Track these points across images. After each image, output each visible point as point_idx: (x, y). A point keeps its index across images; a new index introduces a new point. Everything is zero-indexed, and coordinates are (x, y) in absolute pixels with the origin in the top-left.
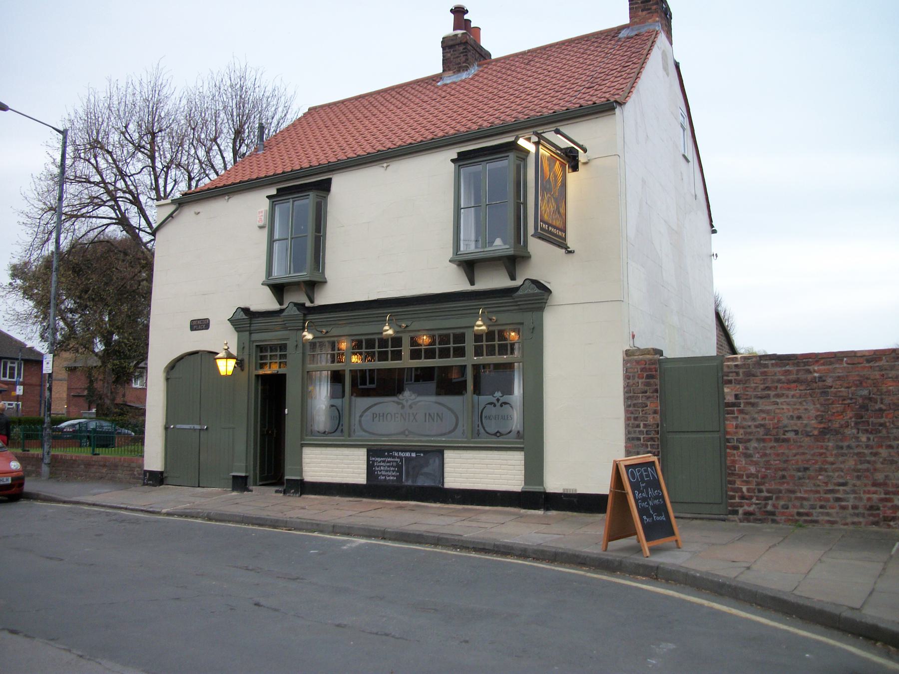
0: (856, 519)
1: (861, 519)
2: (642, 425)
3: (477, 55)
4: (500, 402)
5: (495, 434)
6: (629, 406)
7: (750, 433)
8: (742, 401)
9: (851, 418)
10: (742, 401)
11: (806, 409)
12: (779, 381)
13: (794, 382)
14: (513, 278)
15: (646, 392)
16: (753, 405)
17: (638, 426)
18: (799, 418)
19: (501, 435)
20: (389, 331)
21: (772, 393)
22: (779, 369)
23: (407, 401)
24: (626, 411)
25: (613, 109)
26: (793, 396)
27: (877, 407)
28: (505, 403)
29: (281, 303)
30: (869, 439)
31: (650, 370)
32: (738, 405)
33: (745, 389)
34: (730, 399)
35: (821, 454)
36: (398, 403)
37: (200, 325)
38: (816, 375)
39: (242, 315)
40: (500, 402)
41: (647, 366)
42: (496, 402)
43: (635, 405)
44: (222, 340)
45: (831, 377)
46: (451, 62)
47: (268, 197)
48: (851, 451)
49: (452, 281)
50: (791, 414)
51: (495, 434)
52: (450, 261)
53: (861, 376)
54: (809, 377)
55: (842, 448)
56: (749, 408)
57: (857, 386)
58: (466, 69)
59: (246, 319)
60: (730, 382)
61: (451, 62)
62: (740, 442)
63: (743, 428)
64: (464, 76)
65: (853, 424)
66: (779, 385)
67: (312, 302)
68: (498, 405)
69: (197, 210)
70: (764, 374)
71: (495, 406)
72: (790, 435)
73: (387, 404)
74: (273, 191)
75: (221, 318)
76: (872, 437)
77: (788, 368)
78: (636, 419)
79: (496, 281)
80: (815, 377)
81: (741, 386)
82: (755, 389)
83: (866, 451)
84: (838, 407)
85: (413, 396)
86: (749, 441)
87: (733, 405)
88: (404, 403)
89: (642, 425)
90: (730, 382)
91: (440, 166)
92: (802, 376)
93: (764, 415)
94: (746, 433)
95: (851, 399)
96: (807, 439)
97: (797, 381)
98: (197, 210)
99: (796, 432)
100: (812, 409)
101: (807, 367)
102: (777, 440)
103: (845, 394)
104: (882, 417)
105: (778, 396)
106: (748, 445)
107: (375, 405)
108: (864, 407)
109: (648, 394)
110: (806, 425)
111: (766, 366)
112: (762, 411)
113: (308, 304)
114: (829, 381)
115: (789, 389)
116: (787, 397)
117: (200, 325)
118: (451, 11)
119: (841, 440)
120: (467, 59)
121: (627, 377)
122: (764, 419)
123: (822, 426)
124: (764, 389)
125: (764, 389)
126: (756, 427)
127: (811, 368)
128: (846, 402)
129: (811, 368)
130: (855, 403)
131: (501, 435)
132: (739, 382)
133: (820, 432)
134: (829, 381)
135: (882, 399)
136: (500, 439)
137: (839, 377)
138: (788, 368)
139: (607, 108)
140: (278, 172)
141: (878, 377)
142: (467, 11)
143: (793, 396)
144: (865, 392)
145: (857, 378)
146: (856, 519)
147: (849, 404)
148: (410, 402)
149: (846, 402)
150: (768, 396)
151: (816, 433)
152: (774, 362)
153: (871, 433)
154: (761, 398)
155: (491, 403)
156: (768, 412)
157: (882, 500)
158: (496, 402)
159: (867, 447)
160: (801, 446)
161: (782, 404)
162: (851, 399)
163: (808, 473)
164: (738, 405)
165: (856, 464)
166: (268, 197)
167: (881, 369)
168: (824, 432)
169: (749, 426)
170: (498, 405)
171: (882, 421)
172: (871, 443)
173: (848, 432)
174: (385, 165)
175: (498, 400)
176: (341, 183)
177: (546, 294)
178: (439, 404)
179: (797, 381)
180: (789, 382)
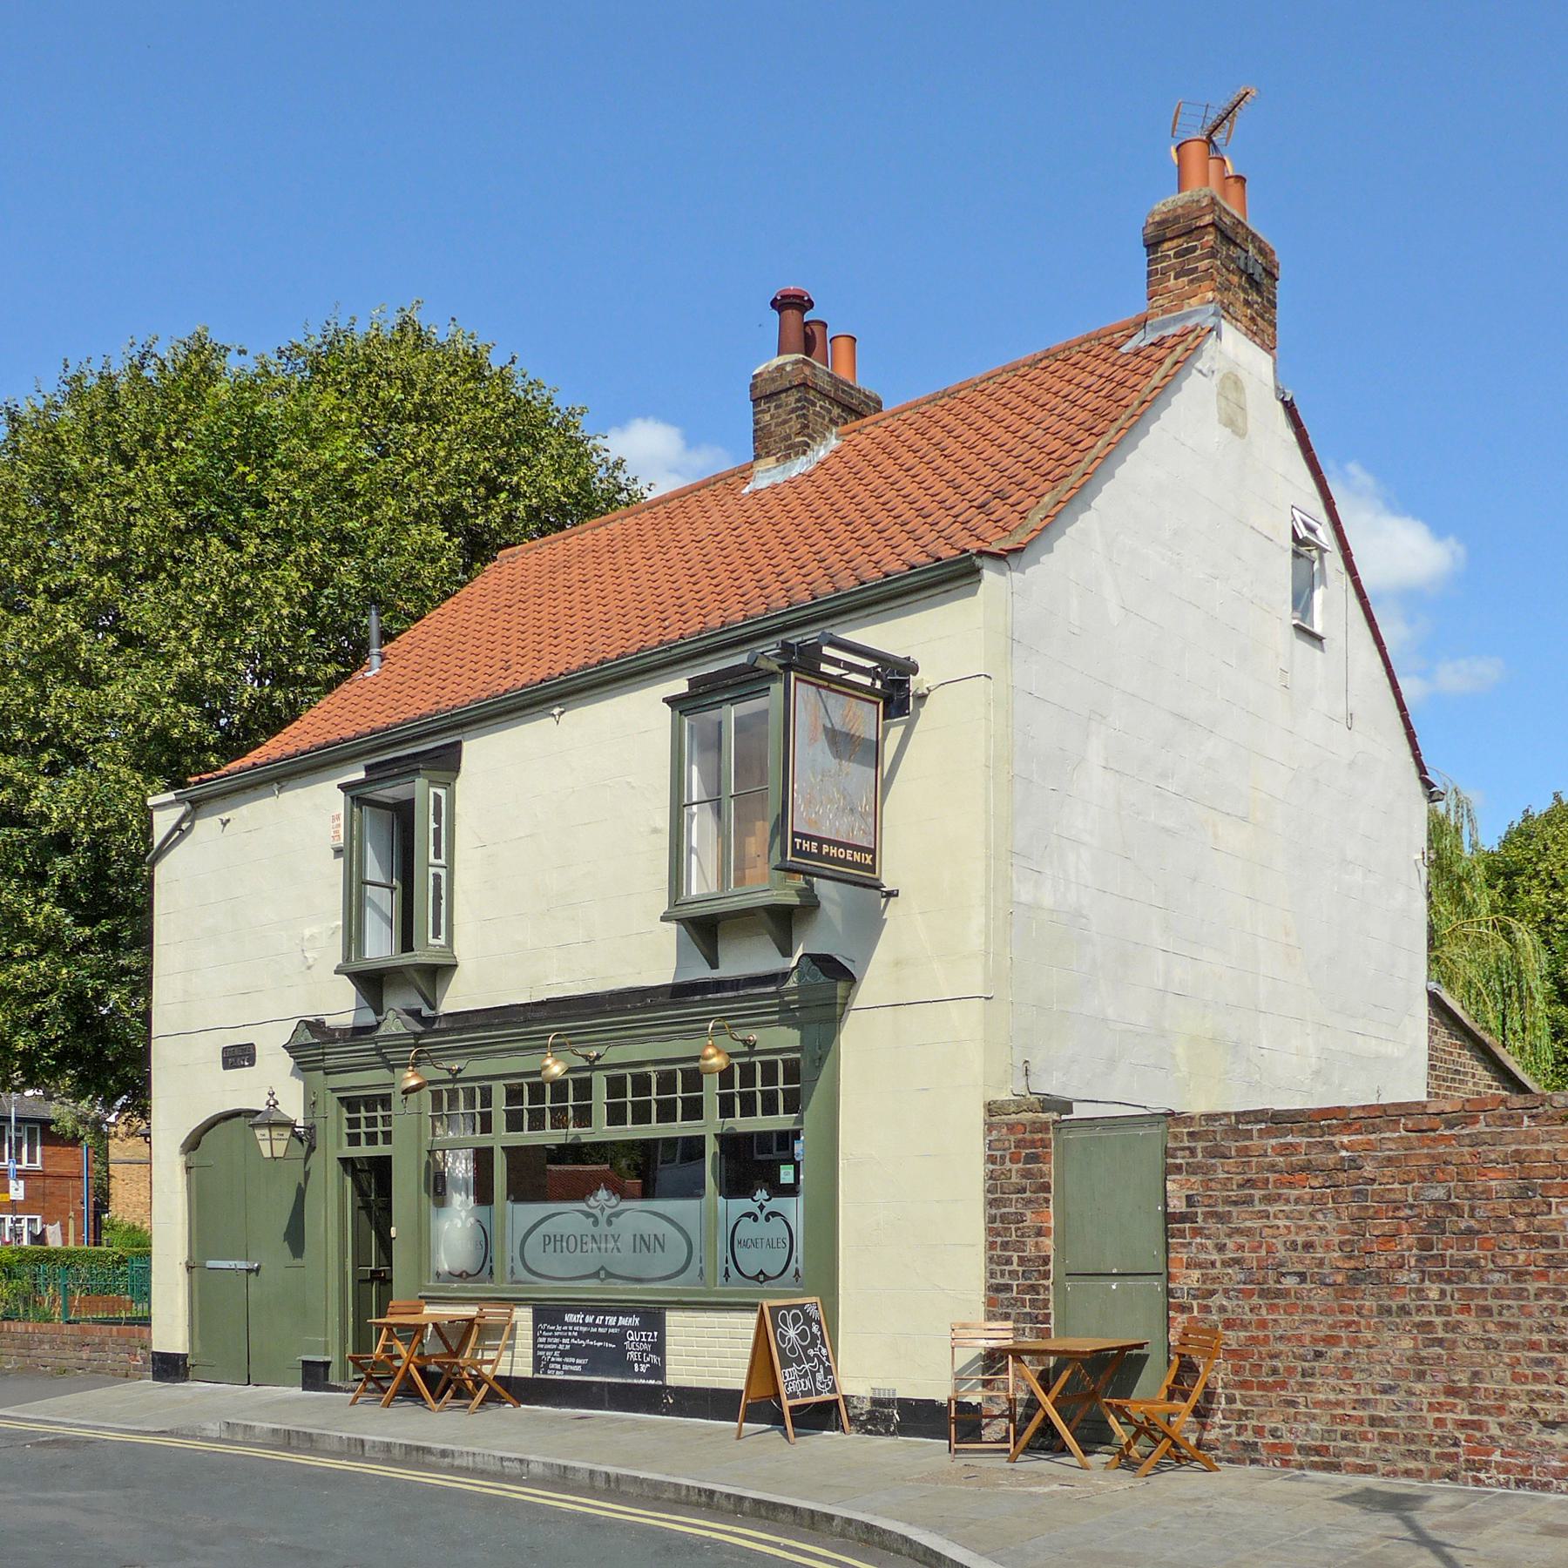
0: (1412, 1465)
1: (1421, 1465)
2: (1015, 1259)
3: (836, 411)
4: (765, 1212)
5: (756, 1278)
6: (992, 1219)
7: (1215, 1279)
8: (1199, 1210)
9: (1410, 1249)
10: (1199, 1210)
11: (1322, 1229)
12: (1272, 1168)
13: (1302, 1170)
14: (787, 952)
15: (1024, 1190)
16: (1222, 1218)
17: (1008, 1261)
18: (1308, 1246)
19: (767, 1278)
20: (556, 1069)
21: (1258, 1194)
22: (1273, 1142)
23: (603, 1210)
24: (990, 1231)
25: (976, 572)
26: (1298, 1200)
27: (1463, 1226)
28: (774, 1214)
29: (378, 1011)
30: (1443, 1293)
31: (1033, 1144)
32: (1191, 1218)
33: (1206, 1185)
34: (1177, 1205)
35: (1349, 1324)
36: (588, 1215)
37: (238, 1056)
38: (1344, 1153)
39: (307, 1037)
40: (765, 1212)
41: (1027, 1136)
42: (758, 1212)
43: (1003, 1218)
44: (276, 1085)
45: (1374, 1158)
46: (770, 435)
47: (667, 701)
48: (1407, 1319)
49: (655, 958)
50: (1292, 1237)
51: (756, 1278)
52: (663, 919)
53: (1433, 1157)
54: (1331, 1159)
55: (1389, 1311)
56: (1212, 1226)
57: (1424, 1178)
58: (804, 448)
59: (314, 1046)
60: (1179, 1168)
61: (770, 435)
62: (1195, 1297)
63: (1199, 1266)
64: (800, 466)
65: (1413, 1263)
66: (1272, 1177)
67: (433, 1007)
68: (761, 1217)
69: (225, 816)
70: (1244, 1152)
71: (756, 1219)
72: (1290, 1282)
73: (567, 1217)
74: (680, 686)
75: (272, 1044)
76: (1448, 1288)
77: (1289, 1139)
78: (1005, 1246)
79: (748, 958)
80: (1343, 1158)
81: (1200, 1177)
82: (1225, 1184)
83: (1438, 1320)
84: (1384, 1225)
85: (614, 1201)
86: (1212, 1293)
87: (1183, 1218)
88: (597, 1212)
89: (1015, 1259)
90: (1179, 1168)
91: (640, 719)
92: (1318, 1157)
93: (1242, 1240)
94: (1205, 1278)
95: (1412, 1207)
96: (1323, 1292)
97: (1307, 1168)
98: (225, 816)
99: (1302, 1276)
100: (1331, 1226)
101: (1326, 1138)
102: (1263, 1294)
103: (1398, 1196)
104: (1472, 1248)
105: (1268, 1199)
106: (1209, 1302)
107: (554, 1215)
108: (1436, 1224)
109: (1028, 1194)
110: (1321, 1263)
111: (1248, 1135)
112: (1239, 1231)
113: (426, 1012)
114: (1369, 1170)
115: (1291, 1185)
116: (1288, 1201)
117: (238, 1056)
118: (774, 303)
119: (1390, 1297)
120: (806, 426)
121: (991, 1159)
122: (1241, 1247)
123: (1352, 1264)
124: (1240, 1186)
125: (1240, 1186)
126: (1225, 1264)
127: (1336, 1139)
128: (1401, 1214)
129: (1336, 1139)
130: (1419, 1216)
131: (767, 1278)
132: (1193, 1169)
133: (1349, 1278)
134: (1369, 1170)
135: (1472, 1209)
136: (765, 1287)
137: (1389, 1159)
138: (1289, 1139)
139: (954, 575)
140: (573, 667)
141: (1467, 1159)
142: (811, 304)
143: (1298, 1200)
144: (1439, 1193)
145: (1426, 1162)
146: (1412, 1465)
147: (1406, 1219)
148: (608, 1211)
149: (1401, 1214)
150: (1249, 1201)
151: (1340, 1279)
152: (1263, 1126)
153: (1449, 1281)
154: (1235, 1203)
155: (748, 1215)
156: (1247, 1232)
157: (1463, 1425)
158: (758, 1212)
159: (1440, 1311)
160: (1311, 1309)
161: (1276, 1217)
162: (1412, 1207)
163: (1322, 1363)
164: (1191, 1218)
165: (1416, 1348)
166: (667, 701)
167: (1475, 1140)
168: (1357, 1277)
169: (1213, 1264)
170: (761, 1217)
171: (1471, 1254)
172: (1448, 1301)
173: (1403, 1277)
174: (556, 711)
175: (761, 1207)
176: (478, 751)
177: (841, 987)
178: (655, 1214)
179: (1307, 1168)
180: (1293, 1170)
